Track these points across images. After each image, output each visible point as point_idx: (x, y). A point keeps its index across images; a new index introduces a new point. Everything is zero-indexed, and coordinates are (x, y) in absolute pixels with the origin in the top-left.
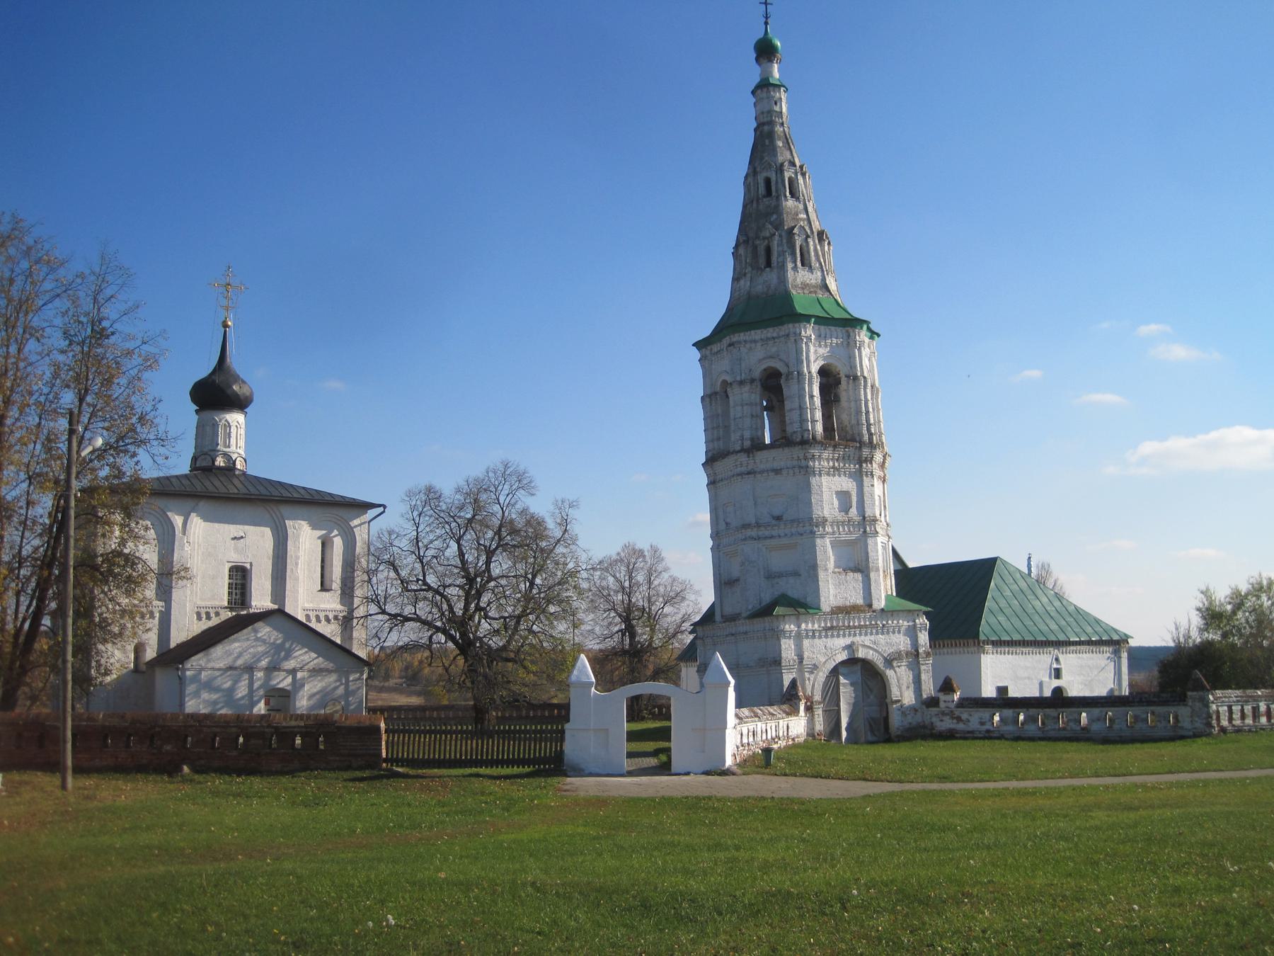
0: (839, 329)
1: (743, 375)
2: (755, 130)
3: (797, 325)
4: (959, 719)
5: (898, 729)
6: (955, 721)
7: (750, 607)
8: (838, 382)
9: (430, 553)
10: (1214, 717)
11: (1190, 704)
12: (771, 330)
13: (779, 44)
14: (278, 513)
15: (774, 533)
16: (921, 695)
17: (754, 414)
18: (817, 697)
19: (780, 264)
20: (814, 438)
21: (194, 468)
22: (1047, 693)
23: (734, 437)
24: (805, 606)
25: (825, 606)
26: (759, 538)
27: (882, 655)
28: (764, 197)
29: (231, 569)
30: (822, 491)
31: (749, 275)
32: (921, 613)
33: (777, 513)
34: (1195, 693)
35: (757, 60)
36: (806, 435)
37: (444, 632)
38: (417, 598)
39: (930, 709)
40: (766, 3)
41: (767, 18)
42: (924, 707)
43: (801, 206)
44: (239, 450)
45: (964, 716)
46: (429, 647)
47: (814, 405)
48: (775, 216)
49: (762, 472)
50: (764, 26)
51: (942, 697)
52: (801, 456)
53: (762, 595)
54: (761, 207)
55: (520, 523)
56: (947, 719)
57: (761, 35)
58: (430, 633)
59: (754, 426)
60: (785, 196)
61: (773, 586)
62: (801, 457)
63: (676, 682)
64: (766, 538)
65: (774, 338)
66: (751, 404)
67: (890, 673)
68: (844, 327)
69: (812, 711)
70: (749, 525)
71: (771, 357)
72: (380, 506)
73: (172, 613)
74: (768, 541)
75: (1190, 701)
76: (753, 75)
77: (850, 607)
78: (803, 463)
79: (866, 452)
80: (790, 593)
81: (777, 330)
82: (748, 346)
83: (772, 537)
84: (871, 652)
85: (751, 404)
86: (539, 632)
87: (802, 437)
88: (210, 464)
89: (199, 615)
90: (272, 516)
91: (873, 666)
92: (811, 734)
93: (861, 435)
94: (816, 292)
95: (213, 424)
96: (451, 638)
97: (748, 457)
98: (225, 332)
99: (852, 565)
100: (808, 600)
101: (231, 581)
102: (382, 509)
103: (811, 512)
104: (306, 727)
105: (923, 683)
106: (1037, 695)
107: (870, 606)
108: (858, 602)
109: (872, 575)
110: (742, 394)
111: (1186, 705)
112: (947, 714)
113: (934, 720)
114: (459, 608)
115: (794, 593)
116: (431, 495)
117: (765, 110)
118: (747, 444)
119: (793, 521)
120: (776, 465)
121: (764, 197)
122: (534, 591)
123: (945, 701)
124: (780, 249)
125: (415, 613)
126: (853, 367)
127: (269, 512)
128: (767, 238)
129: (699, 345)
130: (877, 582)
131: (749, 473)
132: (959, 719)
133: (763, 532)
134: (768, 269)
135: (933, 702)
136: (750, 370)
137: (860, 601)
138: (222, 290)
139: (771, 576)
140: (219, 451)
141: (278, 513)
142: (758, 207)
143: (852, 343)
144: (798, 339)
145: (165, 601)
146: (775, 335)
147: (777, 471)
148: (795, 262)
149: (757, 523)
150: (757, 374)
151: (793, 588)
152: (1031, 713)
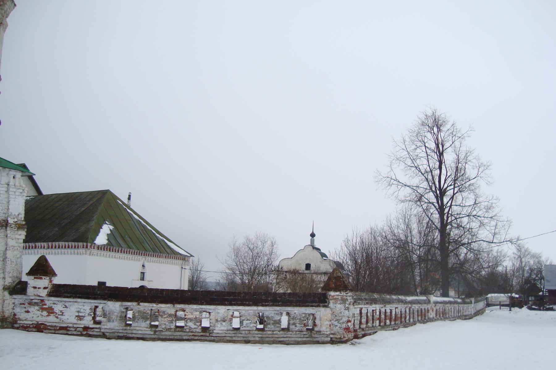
4: (50, 311)
6: (45, 313)
34: (338, 293)
42: (6, 293)
45: (58, 308)
75: (331, 302)
112: (36, 304)
113: (18, 310)
123: (35, 288)
132: (50, 311)
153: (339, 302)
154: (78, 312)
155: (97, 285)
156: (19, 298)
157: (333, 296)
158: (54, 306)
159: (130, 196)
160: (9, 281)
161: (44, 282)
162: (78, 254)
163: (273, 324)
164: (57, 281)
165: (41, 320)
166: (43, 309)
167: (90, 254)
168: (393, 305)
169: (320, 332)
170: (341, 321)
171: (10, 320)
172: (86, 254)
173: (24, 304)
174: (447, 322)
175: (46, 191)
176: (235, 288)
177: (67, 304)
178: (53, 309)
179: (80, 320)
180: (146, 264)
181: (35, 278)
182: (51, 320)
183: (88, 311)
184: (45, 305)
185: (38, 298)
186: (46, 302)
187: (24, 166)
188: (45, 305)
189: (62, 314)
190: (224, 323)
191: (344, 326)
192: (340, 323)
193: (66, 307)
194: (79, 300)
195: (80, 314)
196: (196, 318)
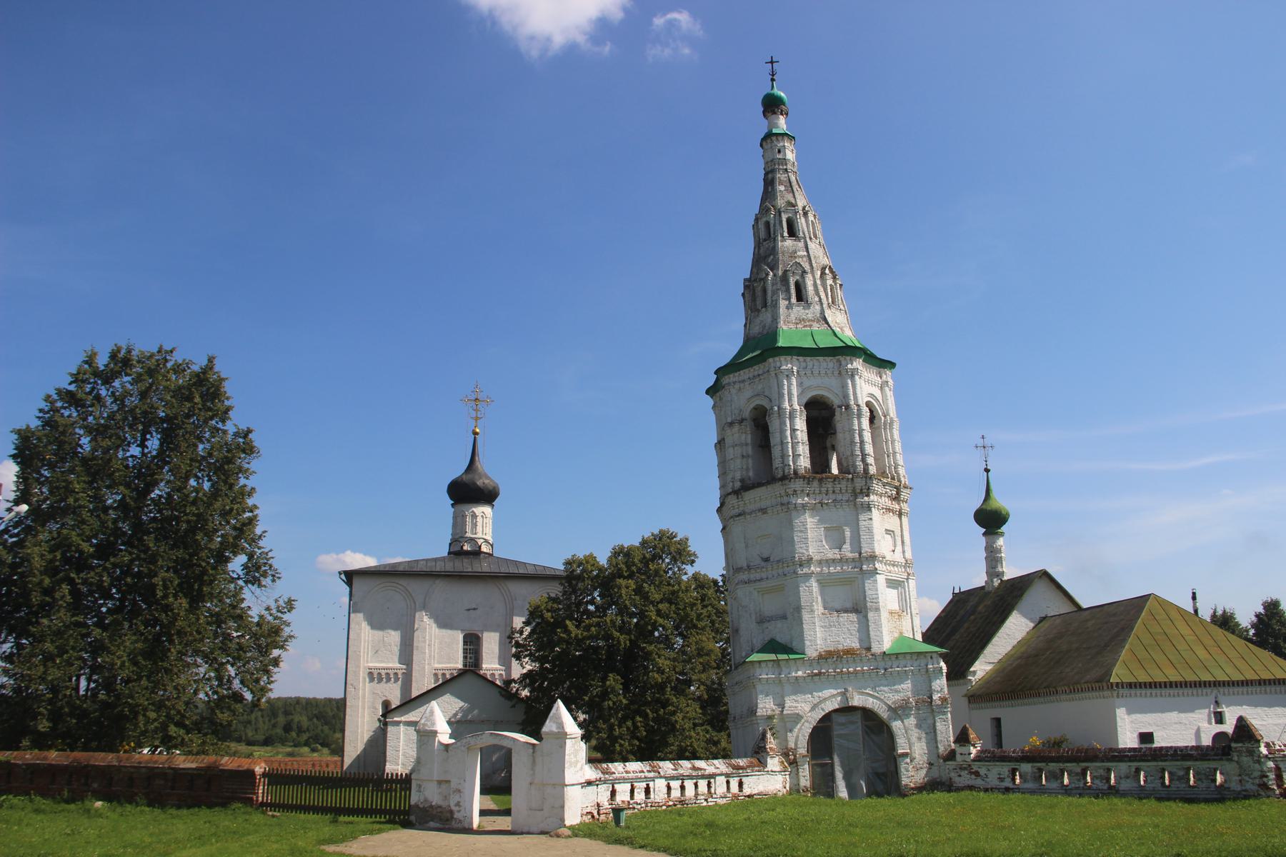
0: (828, 359)
3: (777, 359)
4: (977, 774)
6: (973, 776)
8: (833, 414)
10: (1272, 776)
11: (1236, 758)
12: (756, 367)
13: (782, 94)
14: (505, 588)
15: (764, 575)
16: (937, 747)
17: (745, 454)
18: (803, 750)
19: (774, 303)
20: (796, 472)
21: (449, 553)
22: (1207, 741)
24: (787, 650)
25: (811, 652)
26: (749, 582)
27: (886, 704)
28: (765, 240)
30: (806, 528)
33: (765, 556)
34: (1240, 745)
35: (764, 113)
36: (786, 471)
39: (947, 763)
40: (772, 62)
43: (801, 244)
44: (484, 537)
45: (983, 771)
47: (796, 438)
48: (772, 257)
49: (750, 513)
51: (959, 750)
52: (783, 492)
54: (761, 251)
56: (964, 773)
59: (745, 467)
60: (782, 236)
61: (763, 632)
62: (783, 494)
64: (761, 580)
65: (759, 375)
66: (741, 445)
67: (896, 725)
68: (834, 356)
69: (797, 766)
70: (741, 568)
71: (758, 395)
73: (414, 675)
74: (758, 583)
75: (1235, 754)
76: (762, 127)
77: (843, 651)
78: (785, 500)
79: (859, 483)
80: (778, 639)
81: (762, 367)
82: (737, 386)
83: (761, 580)
84: (871, 699)
85: (741, 445)
87: (784, 472)
88: (460, 549)
89: (371, 674)
90: (501, 592)
91: (872, 712)
92: (795, 789)
93: (855, 466)
94: (811, 326)
95: (463, 516)
97: (738, 498)
98: (475, 438)
99: (849, 605)
100: (793, 645)
101: (465, 647)
103: (793, 551)
105: (938, 732)
106: (1194, 744)
107: (869, 649)
108: (853, 645)
109: (871, 615)
110: (733, 435)
111: (1231, 760)
112: (965, 769)
113: (952, 775)
115: (781, 638)
117: (769, 160)
118: (738, 485)
119: (778, 561)
120: (763, 504)
123: (961, 754)
124: (775, 287)
126: (846, 396)
127: (500, 589)
129: (711, 391)
130: (879, 626)
131: (740, 515)
132: (977, 774)
133: (753, 576)
135: (951, 755)
136: (741, 410)
137: (855, 644)
139: (762, 620)
140: (466, 537)
141: (505, 588)
142: (758, 252)
143: (844, 372)
144: (778, 372)
145: (407, 665)
146: (761, 372)
147: (763, 511)
148: (789, 299)
149: (748, 566)
150: (746, 414)
151: (779, 632)
153: (1244, 754)
154: (999, 774)
155: (514, 618)
157: (1236, 748)
158: (979, 770)
159: (1194, 594)
163: (1178, 780)
165: (970, 783)
167: (1118, 697)
169: (1229, 788)
170: (1252, 776)
171: (948, 783)
173: (955, 769)
175: (1085, 604)
176: (342, 835)
177: (989, 768)
178: (979, 773)
179: (1002, 781)
181: (960, 746)
182: (979, 782)
183: (1007, 773)
184: (972, 769)
185: (965, 763)
186: (973, 767)
188: (972, 769)
189: (987, 777)
190: (1128, 781)
191: (1257, 781)
192: (1251, 779)
193: (989, 770)
194: (998, 763)
195: (1001, 776)
196: (1101, 776)
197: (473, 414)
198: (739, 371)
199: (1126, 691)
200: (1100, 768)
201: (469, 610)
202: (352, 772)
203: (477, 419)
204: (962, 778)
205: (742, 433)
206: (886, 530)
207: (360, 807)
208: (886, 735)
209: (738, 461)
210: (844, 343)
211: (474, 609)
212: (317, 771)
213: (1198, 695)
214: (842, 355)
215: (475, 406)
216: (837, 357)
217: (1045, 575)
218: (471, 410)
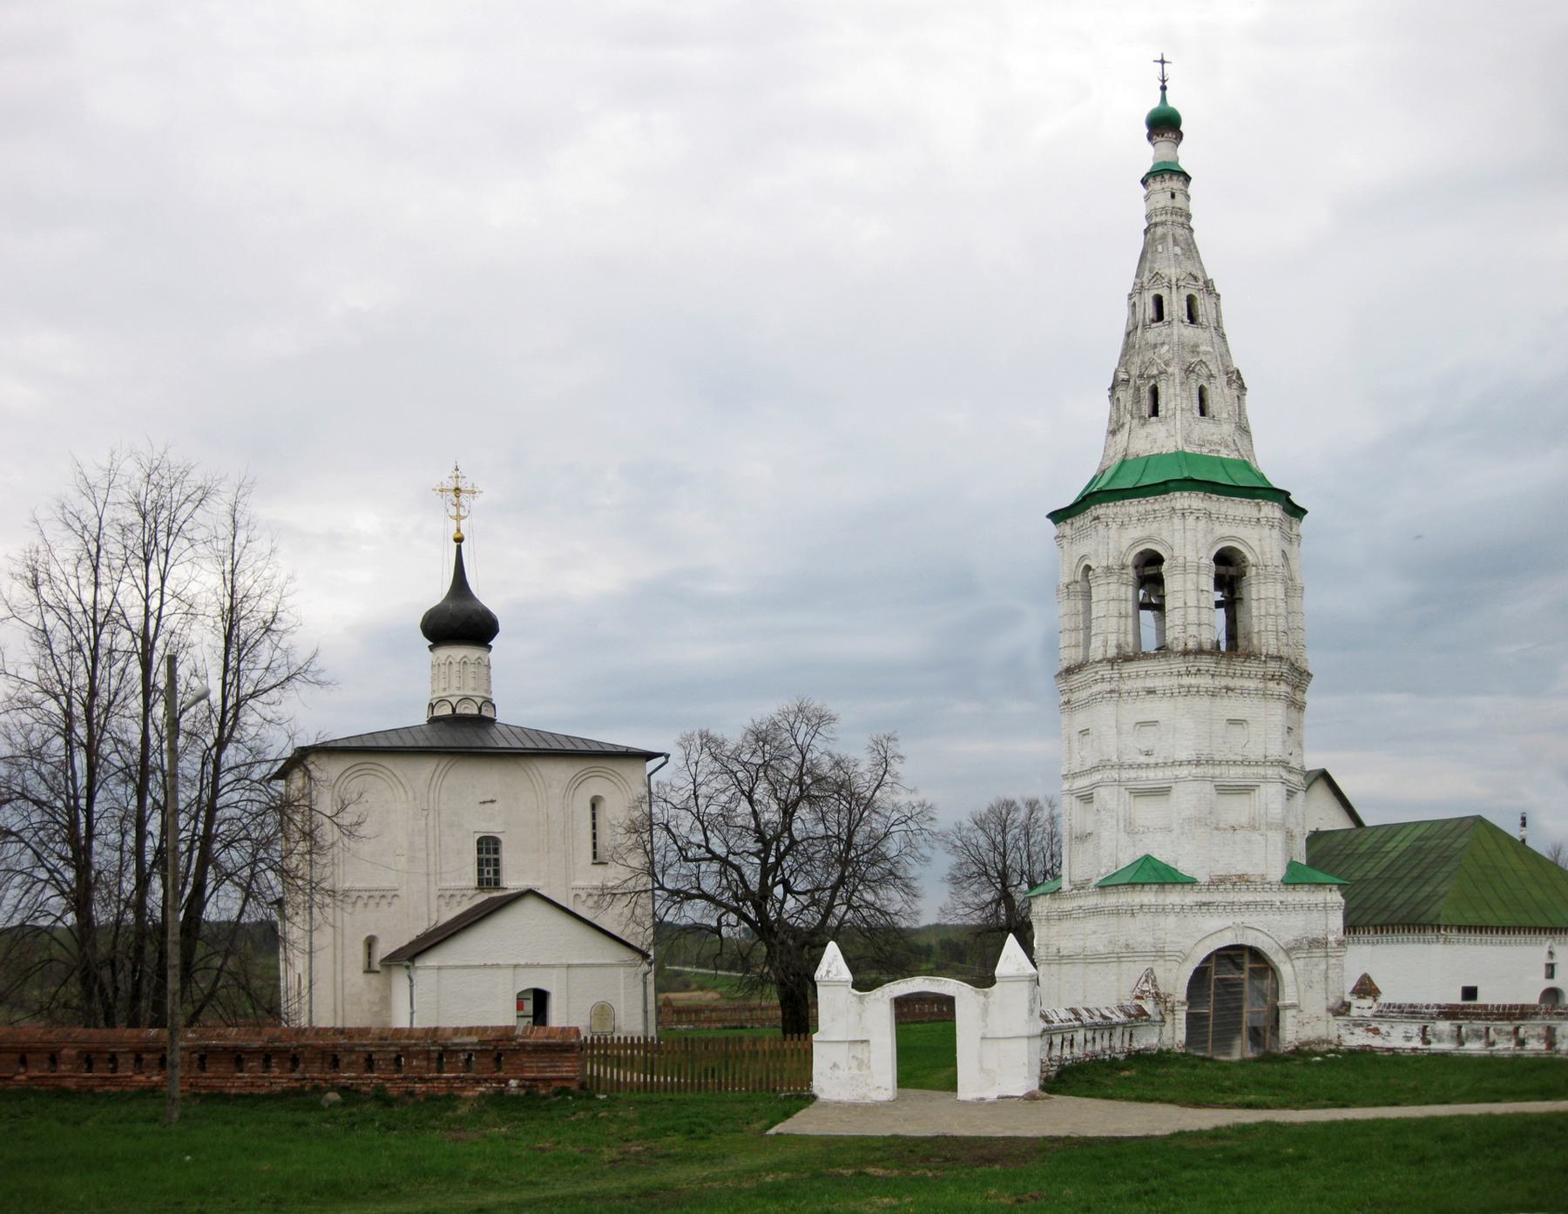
1: (1111, 559)
2: (1146, 232)
5: (1290, 1042)
6: (1370, 1034)
7: (1103, 871)
9: (714, 809)
17: (1123, 612)
23: (1096, 643)
28: (1153, 321)
29: (480, 842)
31: (1127, 426)
32: (1335, 887)
35: (1150, 138)
37: (736, 910)
38: (51, 960)
40: (1163, 62)
41: (1164, 81)
42: (1330, 1015)
45: (1384, 1028)
46: (717, 931)
50: (1160, 92)
53: (1120, 856)
55: (825, 768)
56: (1358, 1031)
57: (1154, 103)
58: (720, 913)
63: (984, 979)
72: (660, 755)
86: (860, 906)
96: (743, 917)
102: (662, 759)
104: (481, 1042)
112: (1361, 1025)
113: (1343, 1032)
114: (753, 879)
116: (707, 740)
118: (1112, 652)
121: (1153, 321)
122: (853, 853)
125: (699, 888)
128: (1154, 377)
132: (1376, 1031)
134: (1153, 419)
138: (452, 495)
152: (1475, 1027)
155: (1223, 610)
156: (1342, 1020)
158: (1379, 1026)
159: (1524, 819)
160: (1332, 1001)
161: (1368, 1002)
162: (1424, 942)
164: (1384, 999)
166: (1368, 1030)
168: (700, 999)
172: (1438, 942)
174: (1398, 1002)
180: (1557, 950)
183: (1416, 1031)
187: (1287, 494)
197: (453, 511)
198: (1123, 499)
199: (1454, 935)
200: (1538, 1025)
201: (484, 802)
202: (622, 1037)
203: (458, 518)
204: (1355, 1037)
205: (1122, 583)
206: (1081, 732)
207: (622, 1080)
208: (1269, 981)
209: (1114, 621)
210: (1233, 481)
211: (492, 801)
212: (616, 1038)
213: (1387, 942)
214: (1263, 498)
215: (455, 499)
216: (1256, 501)
217: (1324, 776)
218: (449, 504)
